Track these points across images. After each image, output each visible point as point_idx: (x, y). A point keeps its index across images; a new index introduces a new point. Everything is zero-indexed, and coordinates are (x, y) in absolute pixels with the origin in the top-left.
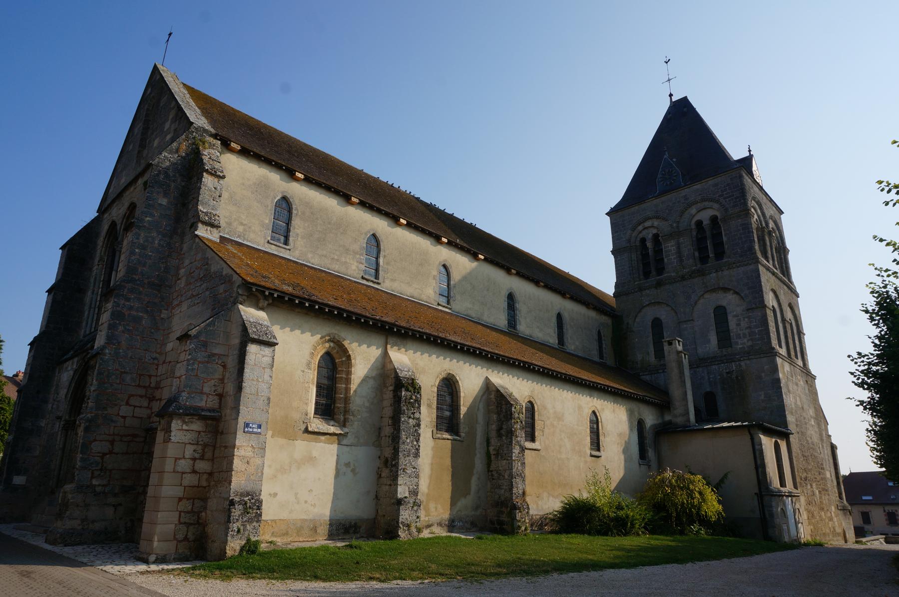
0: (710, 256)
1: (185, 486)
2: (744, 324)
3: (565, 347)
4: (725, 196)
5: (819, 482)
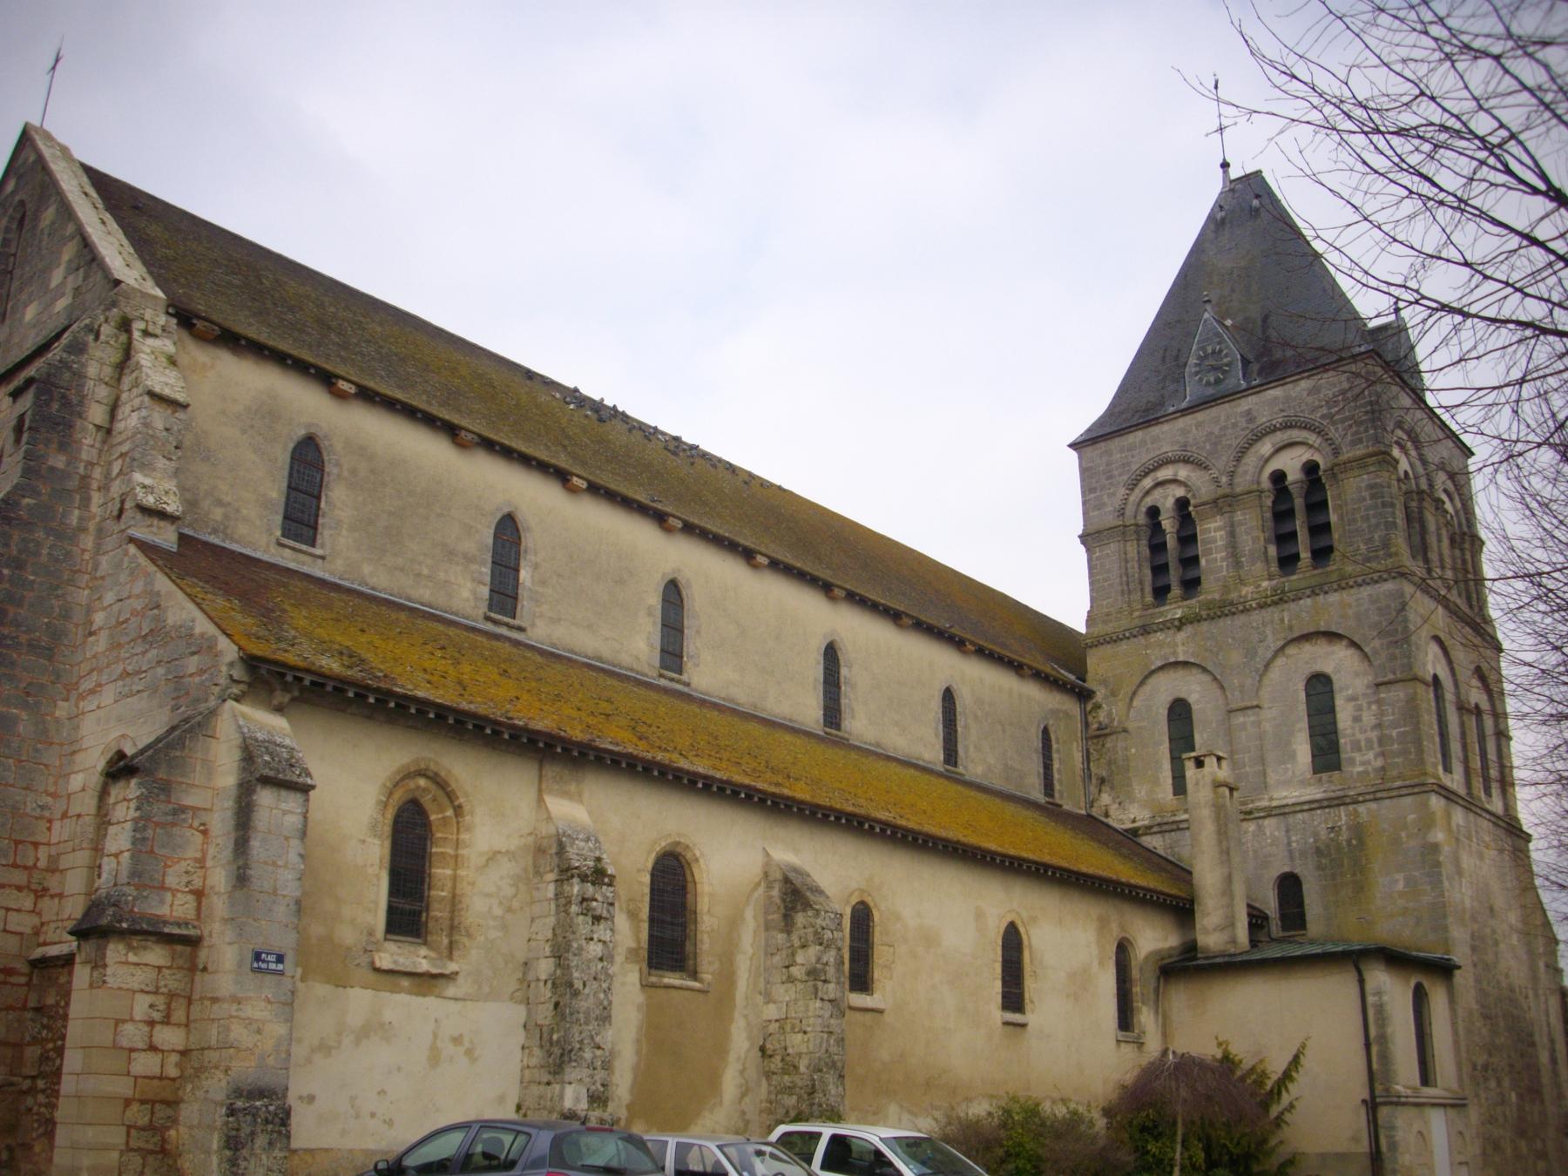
1: (136, 1077)
2: (1368, 718)
3: (960, 769)
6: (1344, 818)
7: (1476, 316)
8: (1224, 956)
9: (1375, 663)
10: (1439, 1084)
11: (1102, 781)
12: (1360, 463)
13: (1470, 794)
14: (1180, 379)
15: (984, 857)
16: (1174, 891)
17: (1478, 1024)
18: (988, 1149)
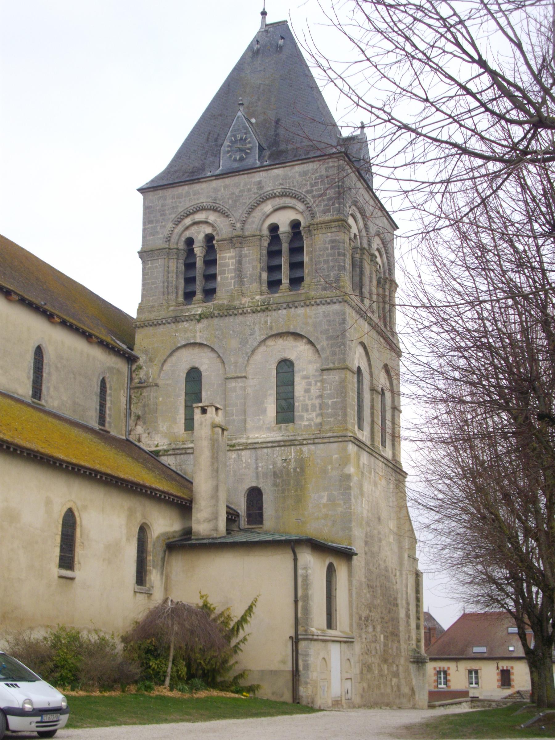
0: (283, 282)
2: (315, 391)
3: (43, 402)
4: (314, 193)
5: (386, 623)
6: (293, 454)
7: (425, 136)
8: (209, 539)
9: (322, 356)
10: (338, 628)
11: (138, 418)
12: (327, 224)
13: (373, 445)
14: (217, 154)
15: (55, 463)
16: (180, 494)
17: (365, 591)
18: (42, 662)
